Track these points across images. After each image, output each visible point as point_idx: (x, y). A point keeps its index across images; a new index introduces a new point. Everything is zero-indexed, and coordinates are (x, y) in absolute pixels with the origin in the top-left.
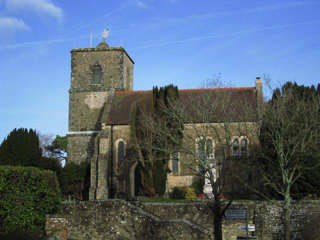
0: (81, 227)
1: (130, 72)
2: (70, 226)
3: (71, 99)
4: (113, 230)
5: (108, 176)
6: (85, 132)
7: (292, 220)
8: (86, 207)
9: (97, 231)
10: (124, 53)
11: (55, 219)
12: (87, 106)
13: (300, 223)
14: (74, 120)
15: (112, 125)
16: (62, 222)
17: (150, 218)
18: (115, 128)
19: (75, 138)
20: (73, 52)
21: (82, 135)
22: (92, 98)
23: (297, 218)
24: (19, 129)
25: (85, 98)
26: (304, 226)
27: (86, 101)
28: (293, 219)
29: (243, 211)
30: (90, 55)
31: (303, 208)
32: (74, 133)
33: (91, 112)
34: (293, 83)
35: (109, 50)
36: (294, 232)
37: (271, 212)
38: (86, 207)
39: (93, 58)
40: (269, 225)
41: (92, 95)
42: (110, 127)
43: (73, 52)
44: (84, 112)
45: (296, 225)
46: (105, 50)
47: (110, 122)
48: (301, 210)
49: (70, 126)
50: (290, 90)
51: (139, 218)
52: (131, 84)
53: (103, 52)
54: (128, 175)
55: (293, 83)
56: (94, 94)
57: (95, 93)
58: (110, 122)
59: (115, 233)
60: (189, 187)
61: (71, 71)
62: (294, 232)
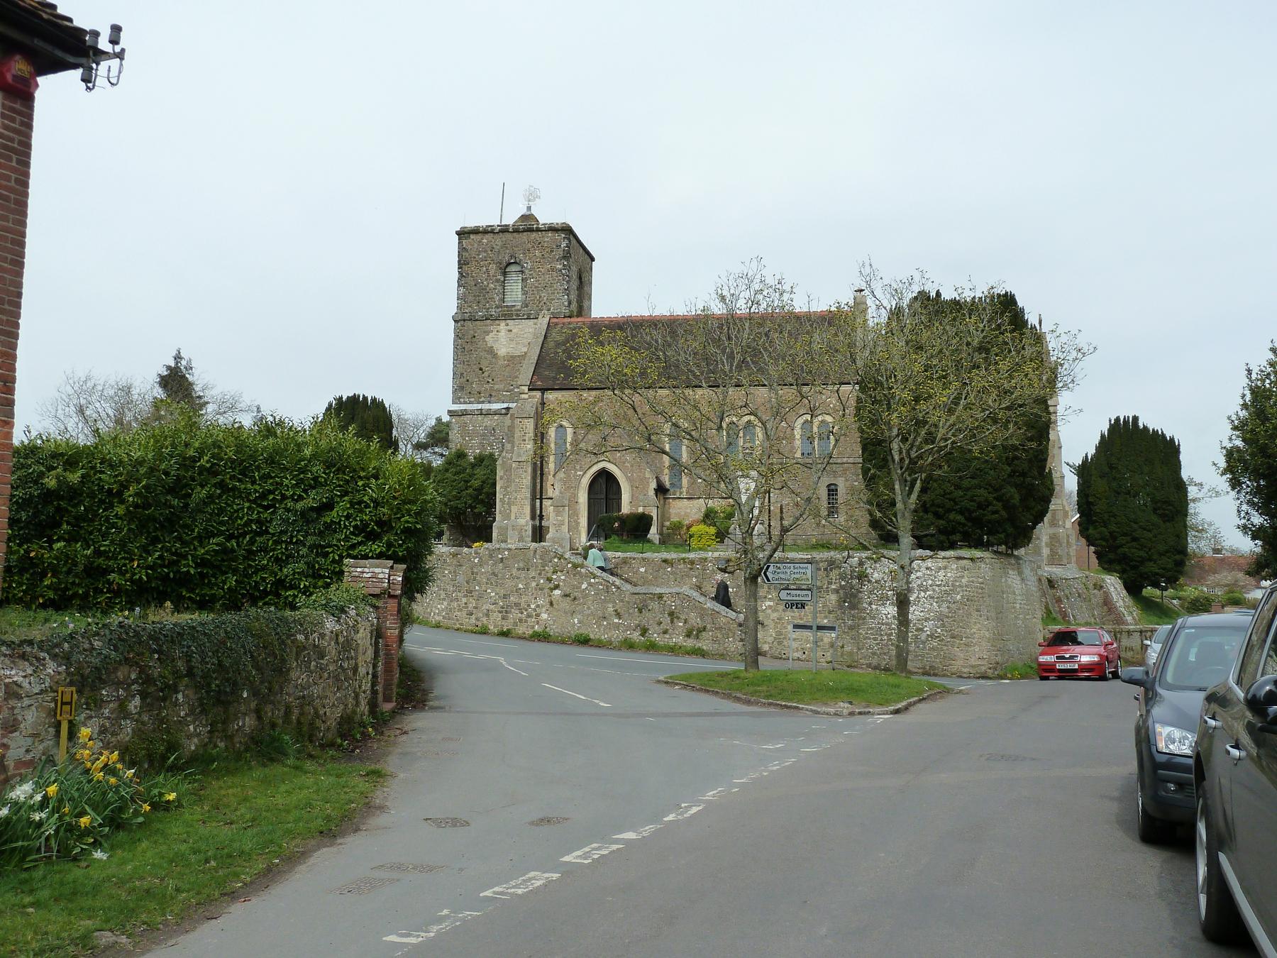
0: (466, 604)
1: (585, 279)
2: (444, 599)
3: (458, 336)
4: (535, 610)
5: (533, 499)
6: (486, 406)
7: (923, 594)
8: (476, 561)
9: (500, 612)
10: (571, 237)
11: (366, 570)
12: (491, 351)
13: (940, 600)
14: (465, 380)
15: (543, 390)
16: (381, 576)
17: (613, 584)
18: (551, 396)
19: (465, 418)
20: (462, 234)
21: (481, 413)
22: (503, 333)
23: (934, 590)
24: (348, 397)
25: (487, 333)
26: (948, 607)
27: (489, 338)
28: (925, 592)
29: (806, 568)
30: (498, 241)
31: (945, 568)
32: (463, 407)
33: (501, 362)
34: (933, 294)
35: (538, 230)
36: (927, 619)
37: (876, 575)
38: (476, 561)
39: (504, 246)
40: (870, 604)
41: (503, 324)
42: (538, 394)
43: (462, 234)
44: (484, 364)
45: (931, 604)
46: (531, 230)
47: (539, 383)
48: (941, 573)
49: (454, 392)
50: (1013, 434)
51: (590, 584)
52: (585, 304)
53: (525, 234)
54: (575, 496)
55: (933, 294)
56: (507, 325)
57: (508, 321)
58: (539, 383)
59: (538, 615)
60: (699, 522)
61: (456, 275)
62: (927, 619)
